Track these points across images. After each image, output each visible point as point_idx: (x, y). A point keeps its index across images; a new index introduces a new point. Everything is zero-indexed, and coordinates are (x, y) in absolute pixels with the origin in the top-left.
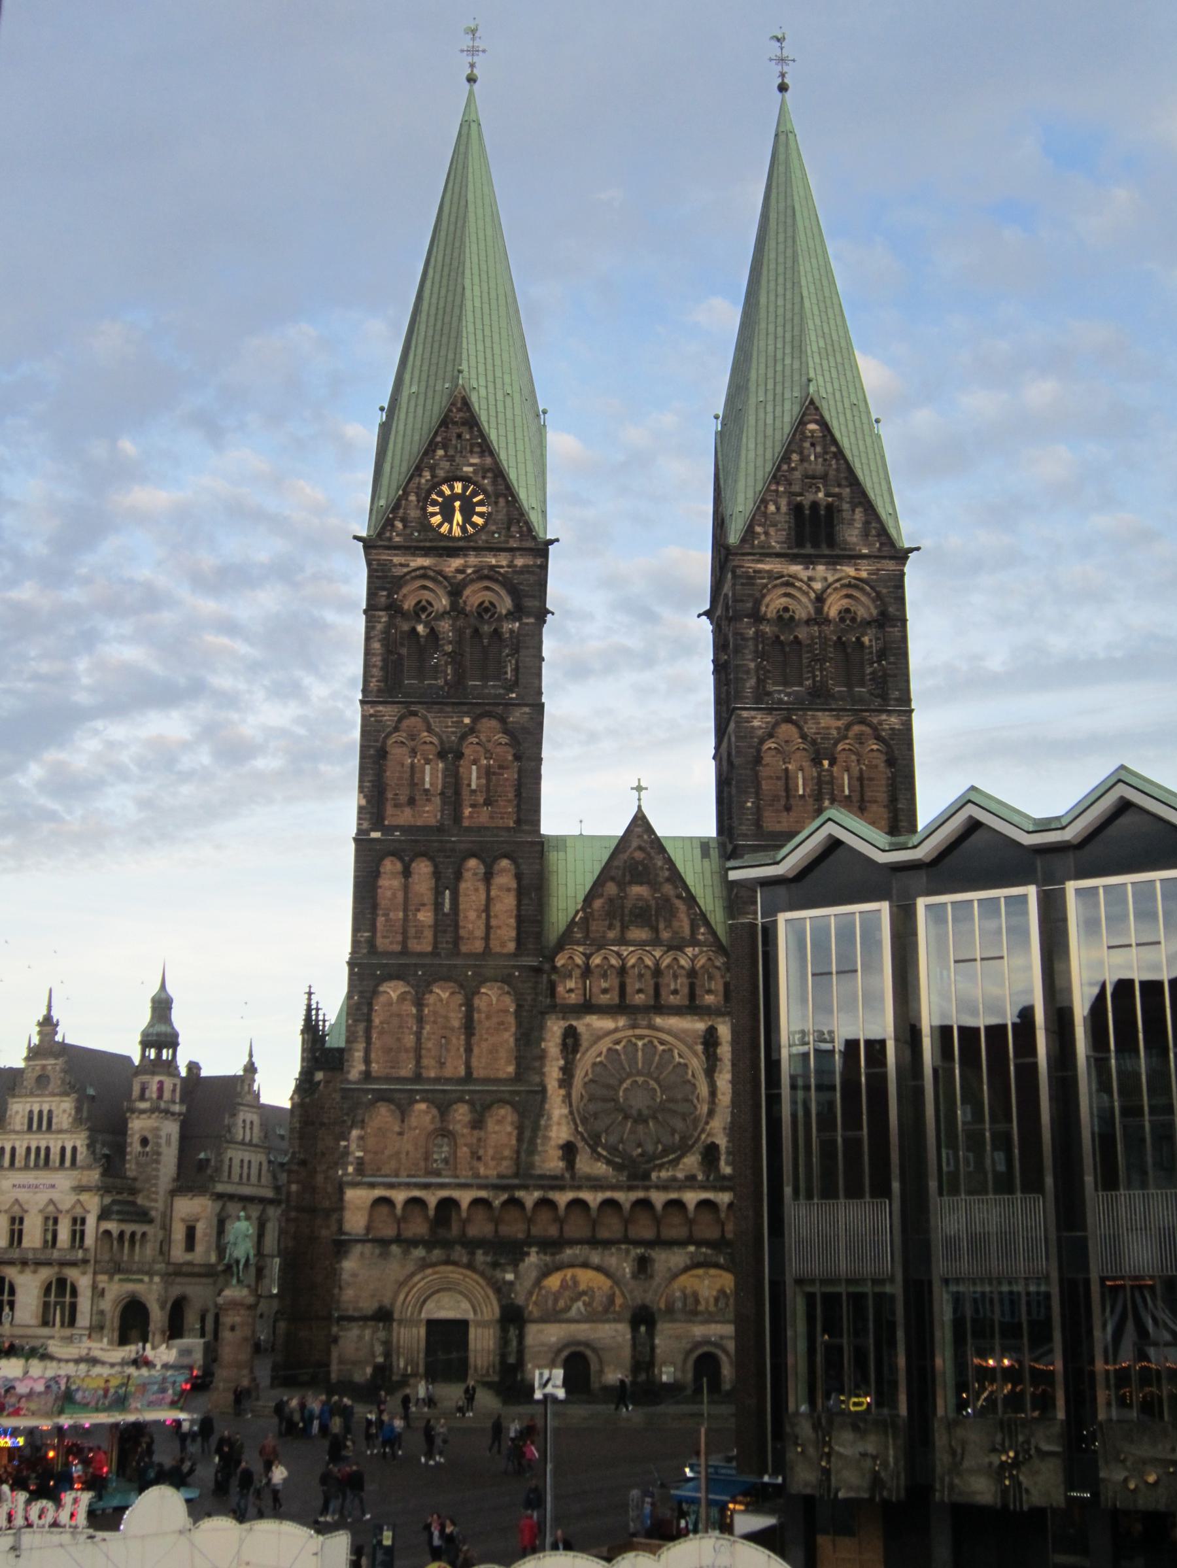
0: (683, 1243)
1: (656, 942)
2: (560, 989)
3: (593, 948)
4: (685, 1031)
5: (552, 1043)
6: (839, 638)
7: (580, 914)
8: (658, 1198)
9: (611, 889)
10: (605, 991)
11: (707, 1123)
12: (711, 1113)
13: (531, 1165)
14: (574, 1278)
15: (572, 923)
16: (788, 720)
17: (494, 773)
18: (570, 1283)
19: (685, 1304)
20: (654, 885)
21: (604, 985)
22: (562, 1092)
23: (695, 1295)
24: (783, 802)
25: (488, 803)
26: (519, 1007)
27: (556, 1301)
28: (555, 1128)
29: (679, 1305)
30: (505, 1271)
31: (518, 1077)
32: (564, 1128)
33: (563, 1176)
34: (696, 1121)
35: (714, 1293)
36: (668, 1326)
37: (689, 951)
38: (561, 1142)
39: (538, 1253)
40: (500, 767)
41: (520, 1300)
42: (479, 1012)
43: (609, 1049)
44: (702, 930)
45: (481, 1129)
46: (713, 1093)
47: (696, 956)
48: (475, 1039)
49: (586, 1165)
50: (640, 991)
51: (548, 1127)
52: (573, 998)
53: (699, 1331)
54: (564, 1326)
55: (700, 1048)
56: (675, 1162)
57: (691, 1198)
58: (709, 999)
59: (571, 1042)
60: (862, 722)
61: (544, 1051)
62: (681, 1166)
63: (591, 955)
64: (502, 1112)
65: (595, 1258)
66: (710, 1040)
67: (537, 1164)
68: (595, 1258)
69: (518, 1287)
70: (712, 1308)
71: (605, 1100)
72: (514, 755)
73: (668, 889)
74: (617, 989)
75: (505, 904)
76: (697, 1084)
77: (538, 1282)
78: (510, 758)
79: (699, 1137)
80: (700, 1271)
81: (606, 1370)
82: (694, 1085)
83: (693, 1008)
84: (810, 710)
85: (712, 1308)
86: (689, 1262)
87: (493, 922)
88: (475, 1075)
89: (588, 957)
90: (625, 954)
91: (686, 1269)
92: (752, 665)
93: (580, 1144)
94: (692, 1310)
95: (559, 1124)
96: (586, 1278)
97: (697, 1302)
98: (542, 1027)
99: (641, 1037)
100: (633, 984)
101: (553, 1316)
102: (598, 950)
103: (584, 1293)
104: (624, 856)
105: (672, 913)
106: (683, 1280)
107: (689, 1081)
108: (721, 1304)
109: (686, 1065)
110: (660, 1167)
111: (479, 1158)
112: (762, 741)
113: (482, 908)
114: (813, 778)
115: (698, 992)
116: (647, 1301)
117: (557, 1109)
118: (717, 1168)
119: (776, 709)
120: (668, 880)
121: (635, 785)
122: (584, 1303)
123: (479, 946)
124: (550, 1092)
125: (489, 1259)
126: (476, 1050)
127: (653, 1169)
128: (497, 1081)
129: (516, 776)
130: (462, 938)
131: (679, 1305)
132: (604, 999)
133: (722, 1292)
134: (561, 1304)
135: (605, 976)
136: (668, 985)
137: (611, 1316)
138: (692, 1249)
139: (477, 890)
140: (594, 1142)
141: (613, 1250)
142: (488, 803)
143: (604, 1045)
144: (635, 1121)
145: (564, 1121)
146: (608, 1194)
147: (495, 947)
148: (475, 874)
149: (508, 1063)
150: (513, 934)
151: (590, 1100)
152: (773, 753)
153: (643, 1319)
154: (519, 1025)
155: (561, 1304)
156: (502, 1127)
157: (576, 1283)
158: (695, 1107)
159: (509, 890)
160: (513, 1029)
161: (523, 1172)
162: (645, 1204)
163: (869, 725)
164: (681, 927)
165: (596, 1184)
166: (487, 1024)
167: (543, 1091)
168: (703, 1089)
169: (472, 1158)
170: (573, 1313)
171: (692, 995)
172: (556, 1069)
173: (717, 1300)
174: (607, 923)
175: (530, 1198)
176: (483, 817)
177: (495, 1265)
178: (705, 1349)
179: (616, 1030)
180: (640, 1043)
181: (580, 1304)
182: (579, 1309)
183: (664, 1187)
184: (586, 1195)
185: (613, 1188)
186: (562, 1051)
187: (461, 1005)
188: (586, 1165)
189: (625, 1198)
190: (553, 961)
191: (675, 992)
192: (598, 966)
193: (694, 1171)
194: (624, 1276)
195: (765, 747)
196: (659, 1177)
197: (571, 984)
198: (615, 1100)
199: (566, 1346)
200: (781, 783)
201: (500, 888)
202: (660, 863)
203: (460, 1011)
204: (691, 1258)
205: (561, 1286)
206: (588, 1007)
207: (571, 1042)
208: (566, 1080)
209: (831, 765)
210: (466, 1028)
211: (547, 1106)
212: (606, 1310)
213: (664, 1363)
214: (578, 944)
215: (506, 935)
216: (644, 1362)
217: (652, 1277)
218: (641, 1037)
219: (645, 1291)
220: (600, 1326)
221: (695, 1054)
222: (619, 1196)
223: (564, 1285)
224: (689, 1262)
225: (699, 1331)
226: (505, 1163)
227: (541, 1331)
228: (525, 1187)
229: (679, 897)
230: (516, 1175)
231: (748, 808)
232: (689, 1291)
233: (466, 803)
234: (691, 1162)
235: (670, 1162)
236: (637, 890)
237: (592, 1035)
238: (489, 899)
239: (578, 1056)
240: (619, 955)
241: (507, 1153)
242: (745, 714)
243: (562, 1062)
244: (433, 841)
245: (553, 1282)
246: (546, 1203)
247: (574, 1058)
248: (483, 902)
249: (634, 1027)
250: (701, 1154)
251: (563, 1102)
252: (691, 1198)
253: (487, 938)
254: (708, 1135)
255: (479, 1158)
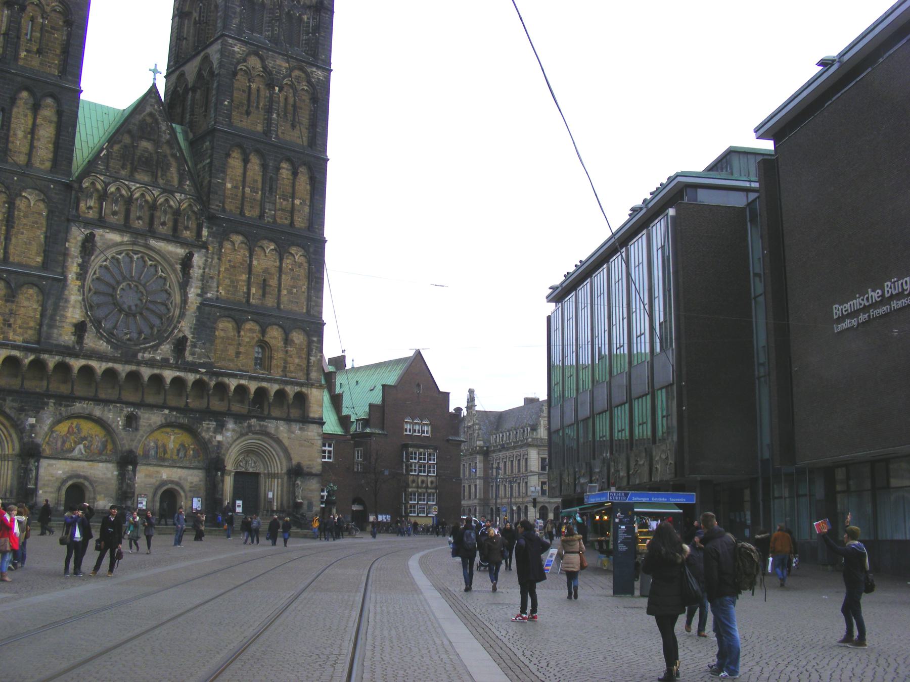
0: (162, 407)
1: (155, 185)
2: (82, 205)
3: (111, 180)
4: (170, 253)
5: (74, 244)
6: (289, 11)
7: (104, 152)
8: (146, 372)
9: (127, 139)
10: (115, 213)
11: (179, 322)
12: (182, 315)
13: (49, 336)
14: (78, 426)
15: (97, 156)
16: (256, 54)
17: (47, 31)
18: (75, 430)
19: (157, 453)
20: (157, 143)
21: (115, 208)
22: (79, 283)
23: (164, 447)
24: (245, 108)
25: (39, 52)
26: (51, 212)
27: (64, 442)
28: (71, 310)
29: (152, 452)
30: (28, 416)
31: (45, 266)
32: (78, 311)
33: (74, 347)
34: (170, 320)
35: (177, 446)
36: (144, 468)
37: (178, 196)
38: (74, 321)
39: (55, 404)
40: (52, 28)
41: (39, 440)
42: (19, 210)
43: (113, 258)
44: (188, 183)
45: (13, 302)
46: (185, 301)
47: (182, 201)
48: (14, 231)
49: (91, 341)
50: (139, 218)
51: (65, 308)
52: (91, 214)
53: (166, 474)
54: (68, 462)
55: (178, 267)
56: (155, 348)
57: (169, 375)
58: (187, 234)
59: (88, 246)
60: (301, 69)
61: (67, 249)
62: (159, 351)
63: (109, 184)
64: (31, 291)
65: (97, 412)
66: (186, 263)
67: (55, 335)
68: (97, 412)
69: (38, 428)
70: (175, 457)
71: (104, 294)
72: (64, 22)
73: (166, 149)
74: (123, 213)
75: (46, 132)
76: (172, 294)
77: (51, 430)
78: (61, 23)
79: (172, 332)
80: (168, 430)
81: (98, 497)
82: (169, 294)
83: (174, 237)
84: (271, 51)
85: (175, 457)
86: (164, 421)
87: (36, 143)
88: (11, 259)
89: (107, 185)
90: (134, 188)
91: (162, 426)
92: (238, 10)
93: (89, 325)
94: (162, 459)
95: (74, 307)
96: (88, 428)
97: (165, 452)
98: (67, 231)
99: (136, 252)
100: (135, 212)
101: (61, 455)
102: (114, 182)
103: (85, 438)
104: (139, 117)
105: (166, 168)
106: (158, 435)
107: (166, 291)
108: (181, 454)
109: (165, 279)
110: (145, 349)
111: (10, 325)
112: (238, 63)
113: (29, 130)
114: (265, 98)
115: (180, 227)
116: (133, 448)
117: (74, 296)
118: (184, 357)
119: (251, 44)
120: (168, 142)
121: (153, 68)
122: (85, 446)
123: (22, 159)
124: (69, 281)
125: (15, 405)
126: (14, 240)
127: (139, 351)
128: (28, 266)
129: (65, 38)
130: (10, 150)
131: (152, 452)
132: (113, 219)
133: (183, 445)
134: (67, 445)
135: (116, 202)
136: (160, 218)
137: (104, 457)
138: (166, 411)
139: (26, 116)
140: (97, 323)
141: (111, 407)
142: (39, 52)
143: (110, 254)
144: (127, 315)
145: (78, 305)
146: (110, 365)
147: (37, 164)
148: (26, 103)
149: (38, 254)
150: (51, 156)
151: (95, 293)
152: (242, 73)
153: (127, 462)
154: (49, 226)
155: (67, 445)
156: (29, 304)
157: (79, 430)
158: (168, 310)
159: (51, 122)
160: (44, 229)
161: (41, 343)
162: (134, 376)
163: (305, 72)
164: (172, 177)
165: (101, 357)
166: (24, 221)
167: (63, 281)
168: (177, 298)
169: (4, 325)
170: (76, 453)
171: (175, 229)
172: (75, 265)
173: (179, 450)
174: (121, 163)
175: (51, 361)
176: (35, 62)
177: (21, 410)
178: (170, 486)
179: (121, 244)
180: (135, 257)
181: (82, 446)
182: (80, 450)
183: (151, 363)
184: (94, 364)
185: (115, 360)
186: (81, 252)
187: (5, 203)
188: (91, 341)
189: (124, 369)
190: (81, 182)
191: (163, 224)
192: (112, 193)
193: (167, 356)
194: (118, 426)
195: (239, 67)
196: (143, 357)
197: (91, 203)
198: (113, 296)
199: (70, 478)
200: (245, 95)
201: (45, 119)
202: (164, 128)
203: (4, 207)
204: (166, 419)
205: (68, 432)
206: (101, 222)
207: (88, 246)
208: (81, 276)
209: (280, 91)
210: (8, 221)
211: (66, 292)
212: (100, 454)
213: (140, 495)
214: (101, 174)
215: (44, 153)
216: (125, 494)
217: (137, 429)
218: (136, 252)
219: (132, 440)
220: (96, 464)
221: (174, 270)
222: (118, 367)
223: (70, 432)
224: (164, 421)
225: (166, 474)
226: (30, 332)
227: (51, 465)
228: (50, 352)
229: (174, 156)
230: (38, 342)
231: (225, 105)
232: (160, 443)
233: (23, 48)
234: (166, 349)
235: (152, 347)
236: (145, 144)
237: (104, 243)
238: (34, 124)
239: (93, 257)
240: (129, 188)
241: (32, 324)
242: (230, 41)
243: (80, 261)
244: (193, 99)
245: (63, 428)
246: (63, 368)
247: (89, 259)
248: (30, 126)
249: (134, 244)
250: (173, 344)
251: (79, 291)
252: (169, 375)
253: (30, 155)
254: (180, 331)
255: (10, 325)
